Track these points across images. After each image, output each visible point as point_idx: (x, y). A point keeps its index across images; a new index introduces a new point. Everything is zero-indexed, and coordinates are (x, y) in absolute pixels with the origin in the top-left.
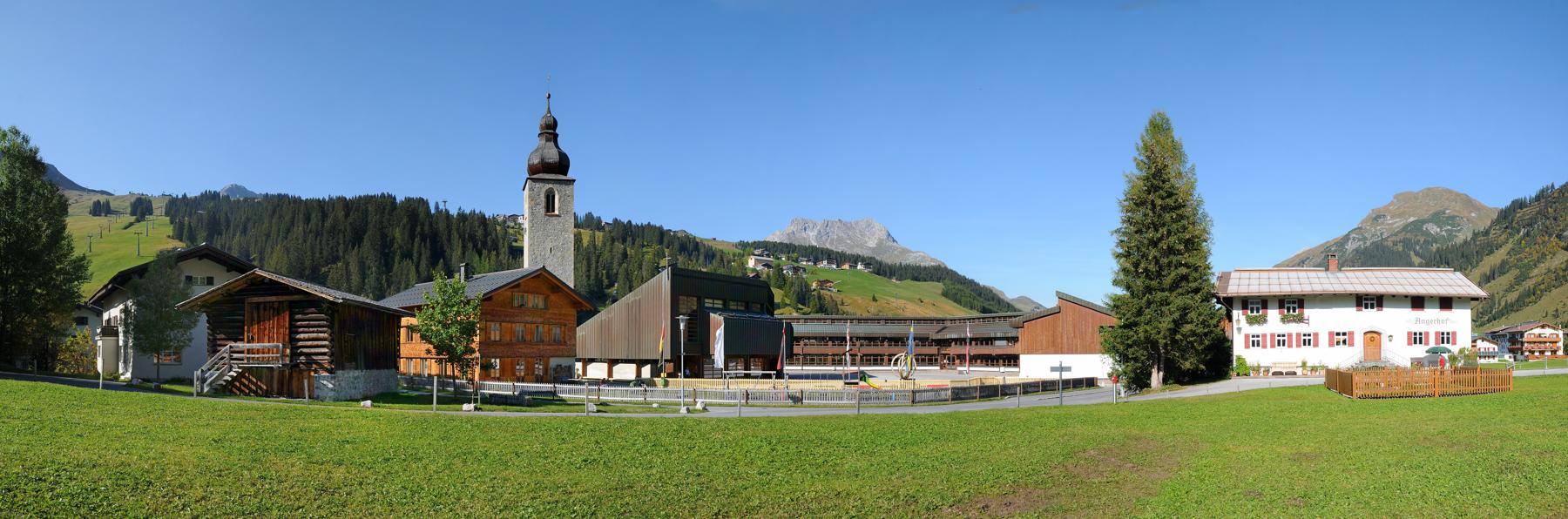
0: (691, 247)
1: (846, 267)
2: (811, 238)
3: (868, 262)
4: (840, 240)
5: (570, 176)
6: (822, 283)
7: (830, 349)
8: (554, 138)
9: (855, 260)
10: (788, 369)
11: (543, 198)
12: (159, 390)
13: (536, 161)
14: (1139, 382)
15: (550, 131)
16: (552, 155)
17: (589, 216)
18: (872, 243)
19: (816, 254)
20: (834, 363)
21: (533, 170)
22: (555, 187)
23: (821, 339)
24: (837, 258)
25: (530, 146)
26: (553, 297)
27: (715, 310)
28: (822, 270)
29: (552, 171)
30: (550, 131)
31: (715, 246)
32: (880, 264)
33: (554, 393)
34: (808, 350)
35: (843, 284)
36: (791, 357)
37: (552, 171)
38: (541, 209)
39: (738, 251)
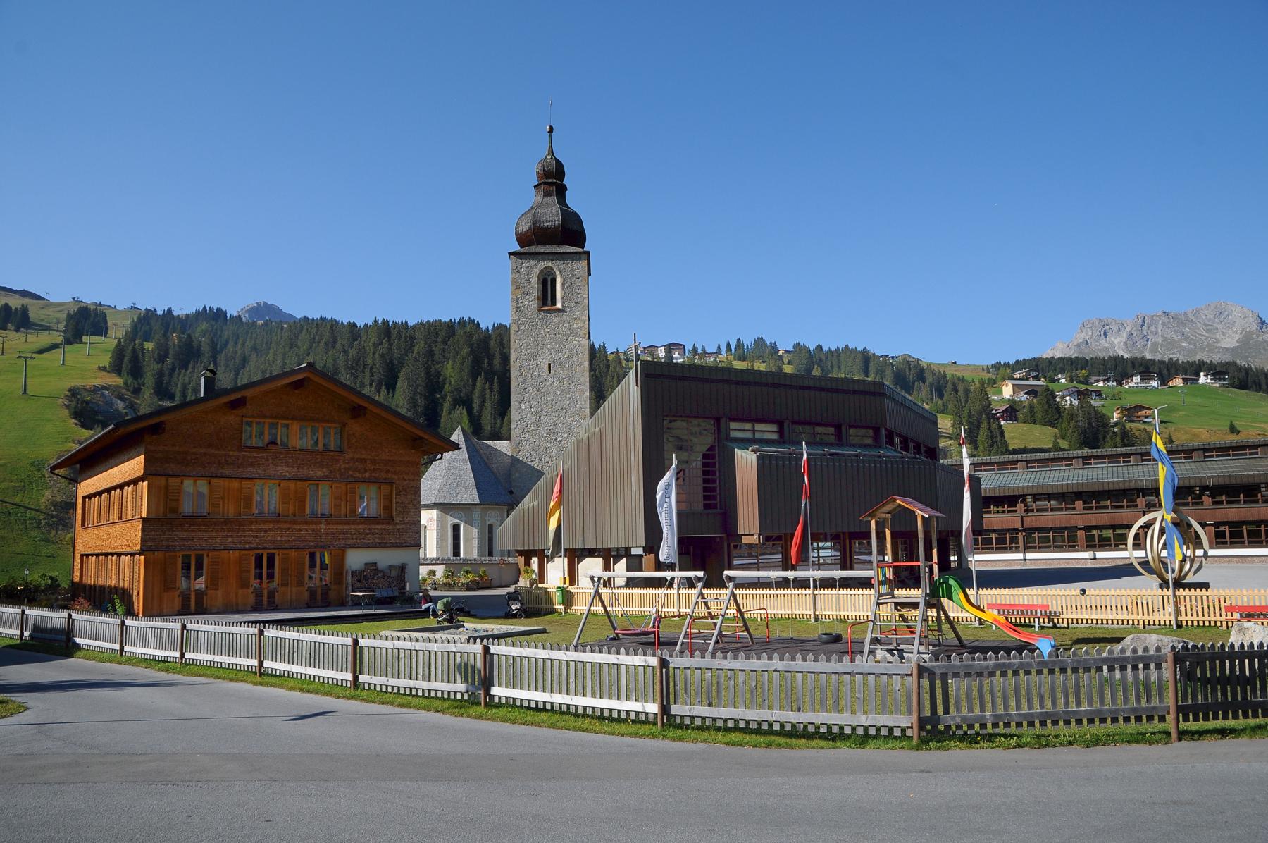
0: (911, 376)
1: (1178, 382)
2: (1118, 346)
3: (1217, 372)
4: (1169, 343)
5: (586, 249)
6: (1131, 412)
7: (1079, 516)
8: (561, 191)
9: (1191, 371)
10: (980, 560)
11: (535, 284)
12: (1042, 742)
13: (526, 227)
14: (1121, 384)
15: (553, 180)
16: (551, 215)
17: (760, 342)
18: (1230, 341)
19: (1119, 369)
20: (1090, 545)
21: (523, 239)
22: (556, 266)
23: (1067, 497)
24: (1164, 371)
25: (523, 200)
26: (355, 427)
27: (744, 443)
28: (1133, 391)
29: (556, 237)
30: (553, 180)
31: (949, 372)
32: (1247, 371)
33: (68, 634)
34: (1034, 520)
35: (1171, 409)
36: (984, 538)
37: (556, 237)
38: (532, 302)
39: (986, 376)
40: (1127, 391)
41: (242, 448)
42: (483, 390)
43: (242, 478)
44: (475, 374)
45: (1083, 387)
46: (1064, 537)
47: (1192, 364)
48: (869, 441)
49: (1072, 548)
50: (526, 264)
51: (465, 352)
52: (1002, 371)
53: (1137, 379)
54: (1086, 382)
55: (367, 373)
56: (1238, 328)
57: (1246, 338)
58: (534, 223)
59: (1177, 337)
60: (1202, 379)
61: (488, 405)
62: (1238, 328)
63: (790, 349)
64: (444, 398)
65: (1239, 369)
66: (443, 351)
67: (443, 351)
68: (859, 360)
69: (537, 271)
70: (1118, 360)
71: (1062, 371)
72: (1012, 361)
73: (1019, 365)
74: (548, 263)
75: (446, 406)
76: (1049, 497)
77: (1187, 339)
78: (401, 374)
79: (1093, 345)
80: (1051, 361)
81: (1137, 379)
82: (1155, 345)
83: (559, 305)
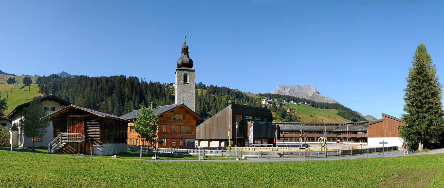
0: (240, 96)
1: (300, 103)
2: (287, 92)
3: (309, 102)
5: (193, 68)
6: (291, 110)
8: (187, 53)
9: (304, 101)
10: (278, 143)
11: (183, 77)
13: (180, 62)
15: (186, 51)
16: (186, 60)
19: (289, 99)
20: (296, 141)
21: (179, 66)
25: (178, 57)
26: (187, 115)
27: (249, 120)
29: (186, 66)
30: (186, 51)
33: (187, 153)
35: (299, 110)
36: (279, 139)
37: (186, 66)
39: (258, 97)
40: (290, 105)
41: (171, 119)
42: (135, 96)
43: (171, 125)
44: (132, 92)
45: (281, 103)
46: (291, 139)
47: (303, 99)
48: (260, 120)
49: (292, 141)
50: (181, 72)
51: (129, 85)
52: (262, 96)
53: (292, 102)
54: (281, 101)
55: (105, 91)
56: (312, 92)
57: (314, 94)
58: (183, 62)
59: (300, 92)
60: (305, 104)
61: (137, 100)
62: (312, 92)
63: (209, 86)
64: (125, 98)
65: (312, 102)
66: (123, 85)
67: (123, 85)
68: (227, 91)
69: (183, 74)
70: (288, 96)
71: (275, 98)
72: (263, 93)
73: (266, 95)
74: (186, 72)
75: (126, 100)
76: (288, 131)
77: (302, 92)
78: (114, 92)
79: (281, 91)
80: (273, 95)
81: (292, 102)
82: (295, 93)
83: (188, 82)
